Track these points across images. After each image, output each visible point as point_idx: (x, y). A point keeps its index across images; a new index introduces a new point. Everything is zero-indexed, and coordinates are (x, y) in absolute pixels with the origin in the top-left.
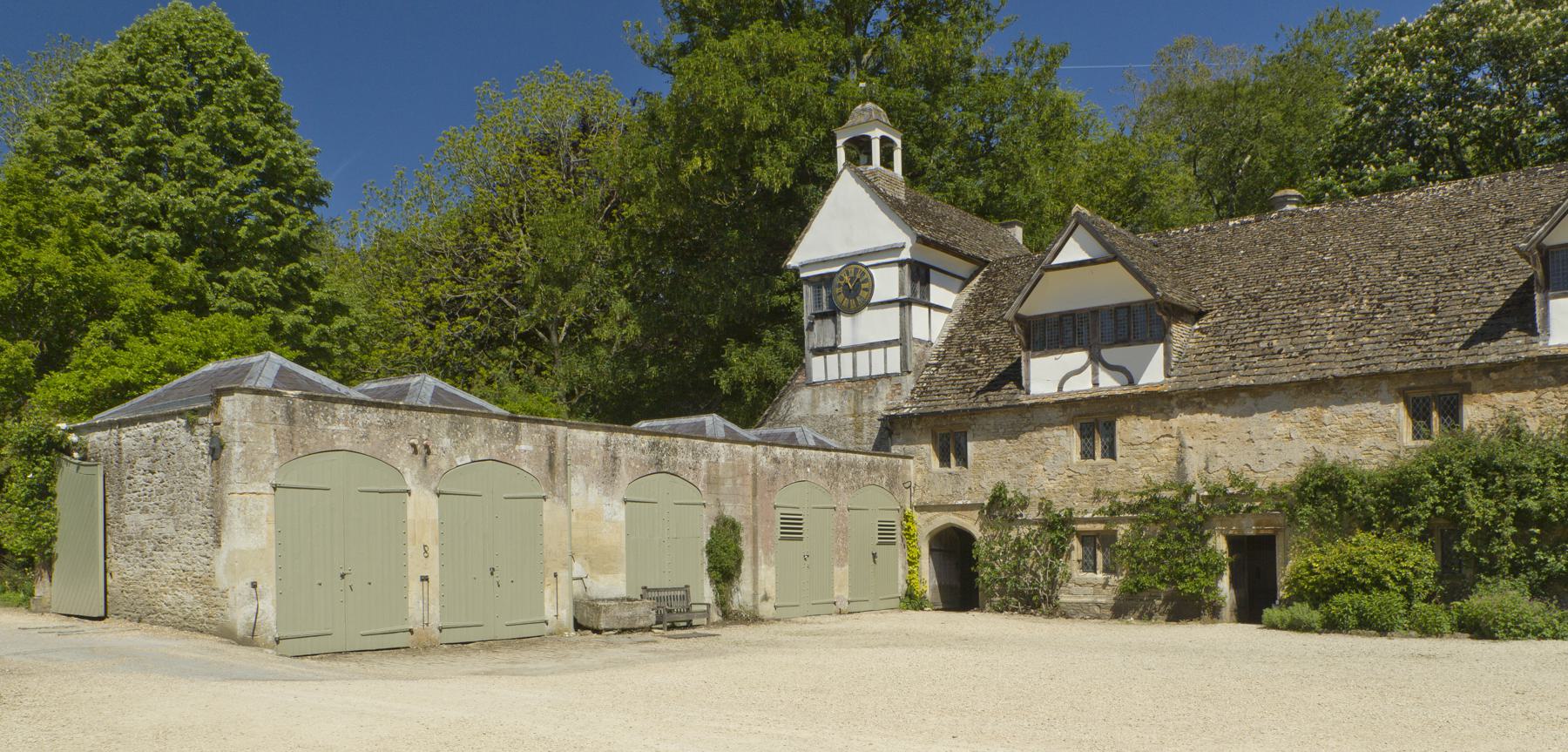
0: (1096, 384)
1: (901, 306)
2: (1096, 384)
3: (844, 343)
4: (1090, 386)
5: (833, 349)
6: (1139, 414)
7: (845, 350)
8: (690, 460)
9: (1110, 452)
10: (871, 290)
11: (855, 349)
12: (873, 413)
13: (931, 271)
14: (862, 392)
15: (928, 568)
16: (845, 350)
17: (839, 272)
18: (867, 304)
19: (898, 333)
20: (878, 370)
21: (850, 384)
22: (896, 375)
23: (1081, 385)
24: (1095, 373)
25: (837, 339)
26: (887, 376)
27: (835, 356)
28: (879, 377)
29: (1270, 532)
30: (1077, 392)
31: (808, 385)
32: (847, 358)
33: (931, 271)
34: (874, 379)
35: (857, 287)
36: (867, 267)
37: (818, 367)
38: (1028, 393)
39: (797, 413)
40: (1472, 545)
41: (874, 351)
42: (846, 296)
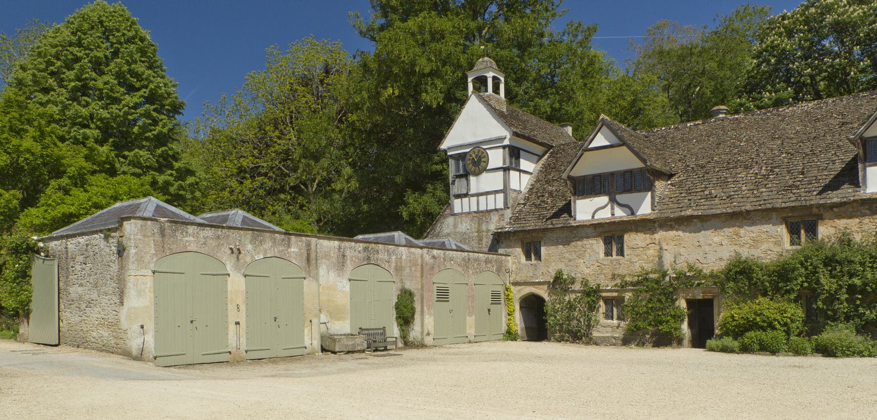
0: (613, 215)
1: (504, 171)
2: (613, 215)
3: (472, 192)
4: (610, 215)
5: (466, 195)
6: (637, 231)
7: (473, 195)
8: (386, 257)
9: (621, 252)
10: (487, 162)
11: (478, 195)
12: (488, 231)
13: (521, 151)
14: (482, 219)
15: (519, 317)
16: (473, 195)
17: (469, 152)
18: (485, 170)
19: (502, 186)
20: (491, 207)
21: (475, 215)
22: (501, 209)
23: (605, 215)
24: (612, 209)
25: (468, 189)
26: (496, 210)
27: (467, 199)
28: (492, 211)
29: (710, 297)
30: (603, 219)
31: (452, 215)
32: (474, 200)
33: (521, 151)
34: (489, 212)
35: (479, 160)
36: (485, 149)
37: (458, 205)
38: (575, 219)
39: (446, 231)
40: (823, 305)
41: (489, 196)
42: (473, 165)
